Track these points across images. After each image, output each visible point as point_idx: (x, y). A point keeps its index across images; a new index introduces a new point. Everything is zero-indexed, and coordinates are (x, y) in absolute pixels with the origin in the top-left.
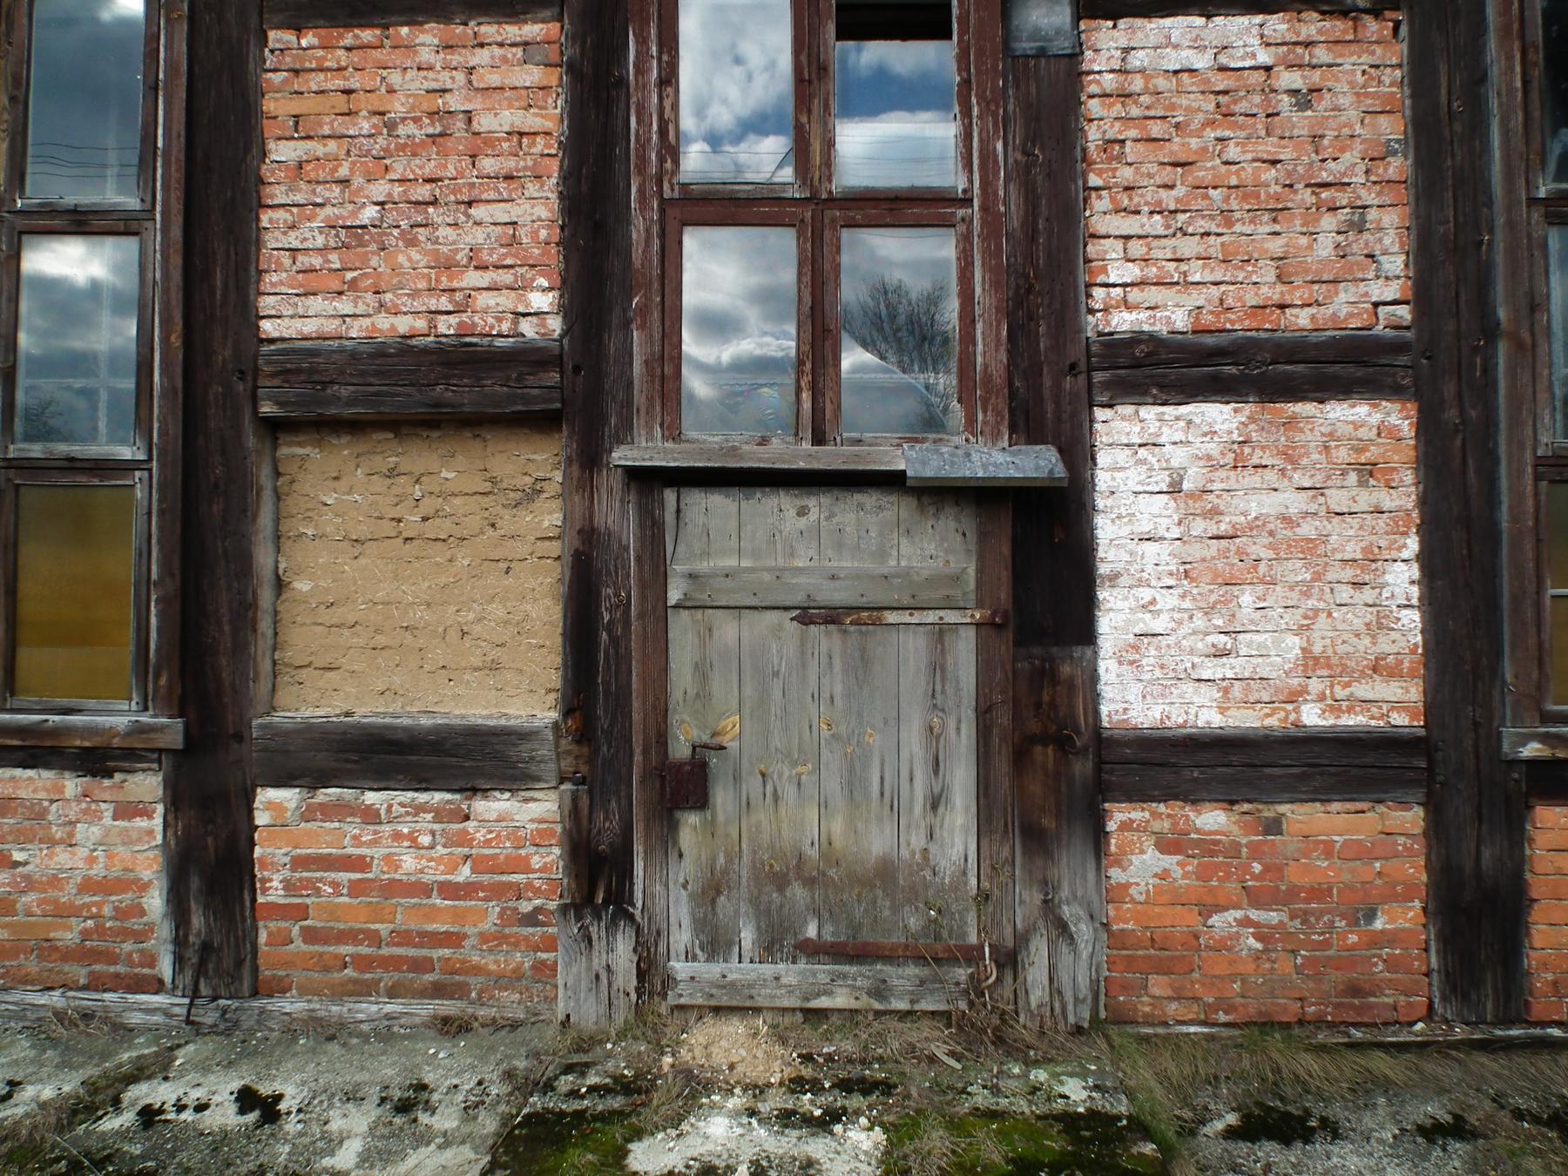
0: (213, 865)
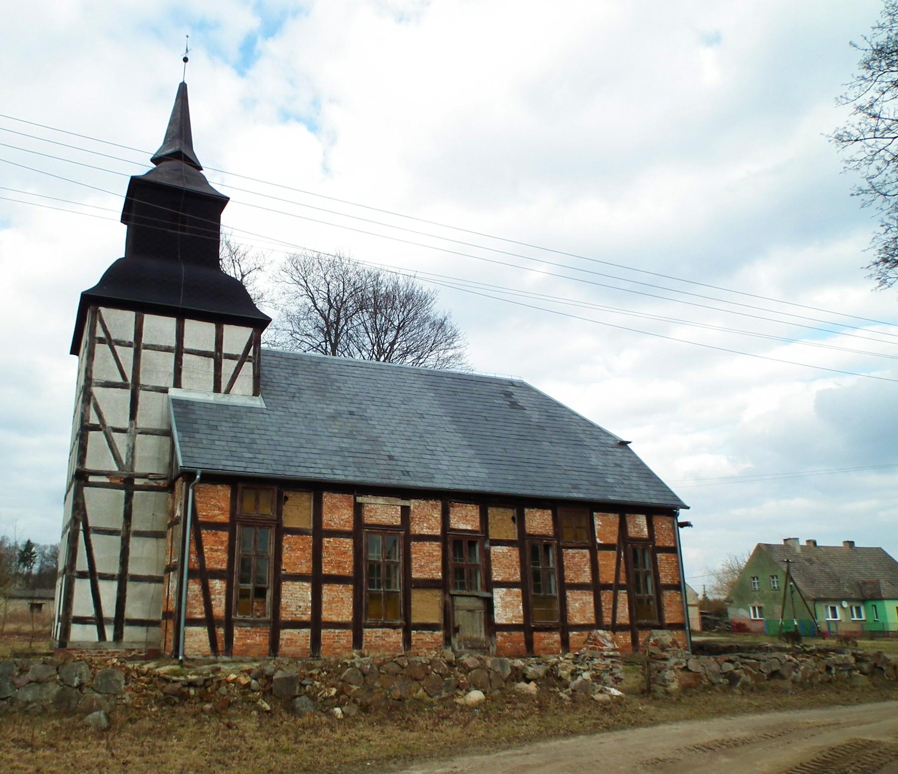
0: (407, 640)
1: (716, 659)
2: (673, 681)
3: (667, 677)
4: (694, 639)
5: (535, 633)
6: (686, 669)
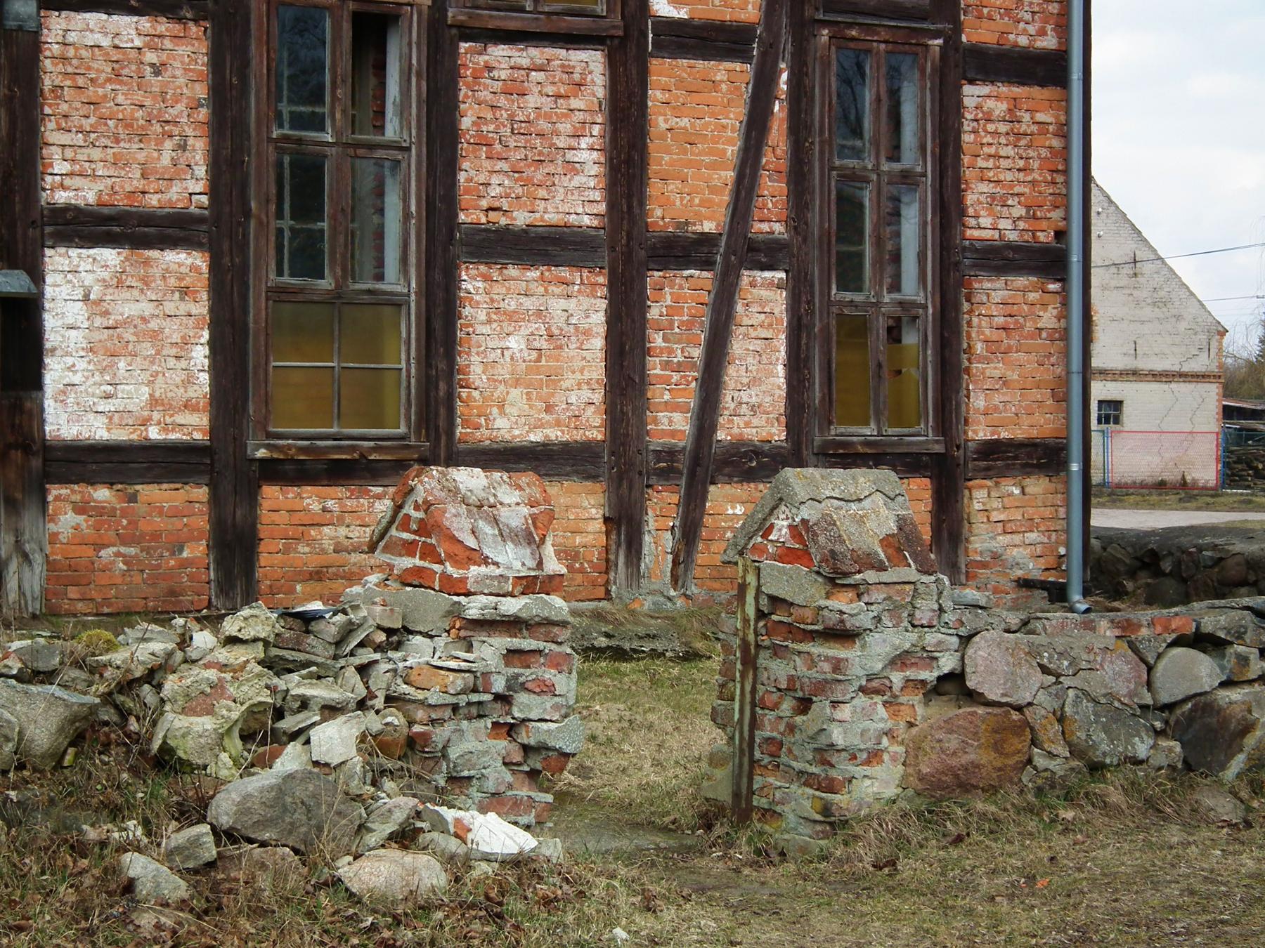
1: (1126, 630)
2: (874, 756)
3: (837, 736)
4: (1103, 519)
5: (272, 495)
6: (954, 685)
